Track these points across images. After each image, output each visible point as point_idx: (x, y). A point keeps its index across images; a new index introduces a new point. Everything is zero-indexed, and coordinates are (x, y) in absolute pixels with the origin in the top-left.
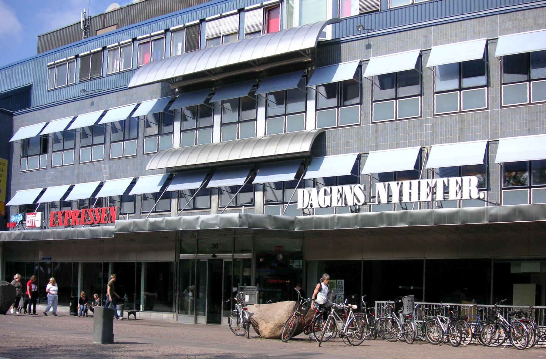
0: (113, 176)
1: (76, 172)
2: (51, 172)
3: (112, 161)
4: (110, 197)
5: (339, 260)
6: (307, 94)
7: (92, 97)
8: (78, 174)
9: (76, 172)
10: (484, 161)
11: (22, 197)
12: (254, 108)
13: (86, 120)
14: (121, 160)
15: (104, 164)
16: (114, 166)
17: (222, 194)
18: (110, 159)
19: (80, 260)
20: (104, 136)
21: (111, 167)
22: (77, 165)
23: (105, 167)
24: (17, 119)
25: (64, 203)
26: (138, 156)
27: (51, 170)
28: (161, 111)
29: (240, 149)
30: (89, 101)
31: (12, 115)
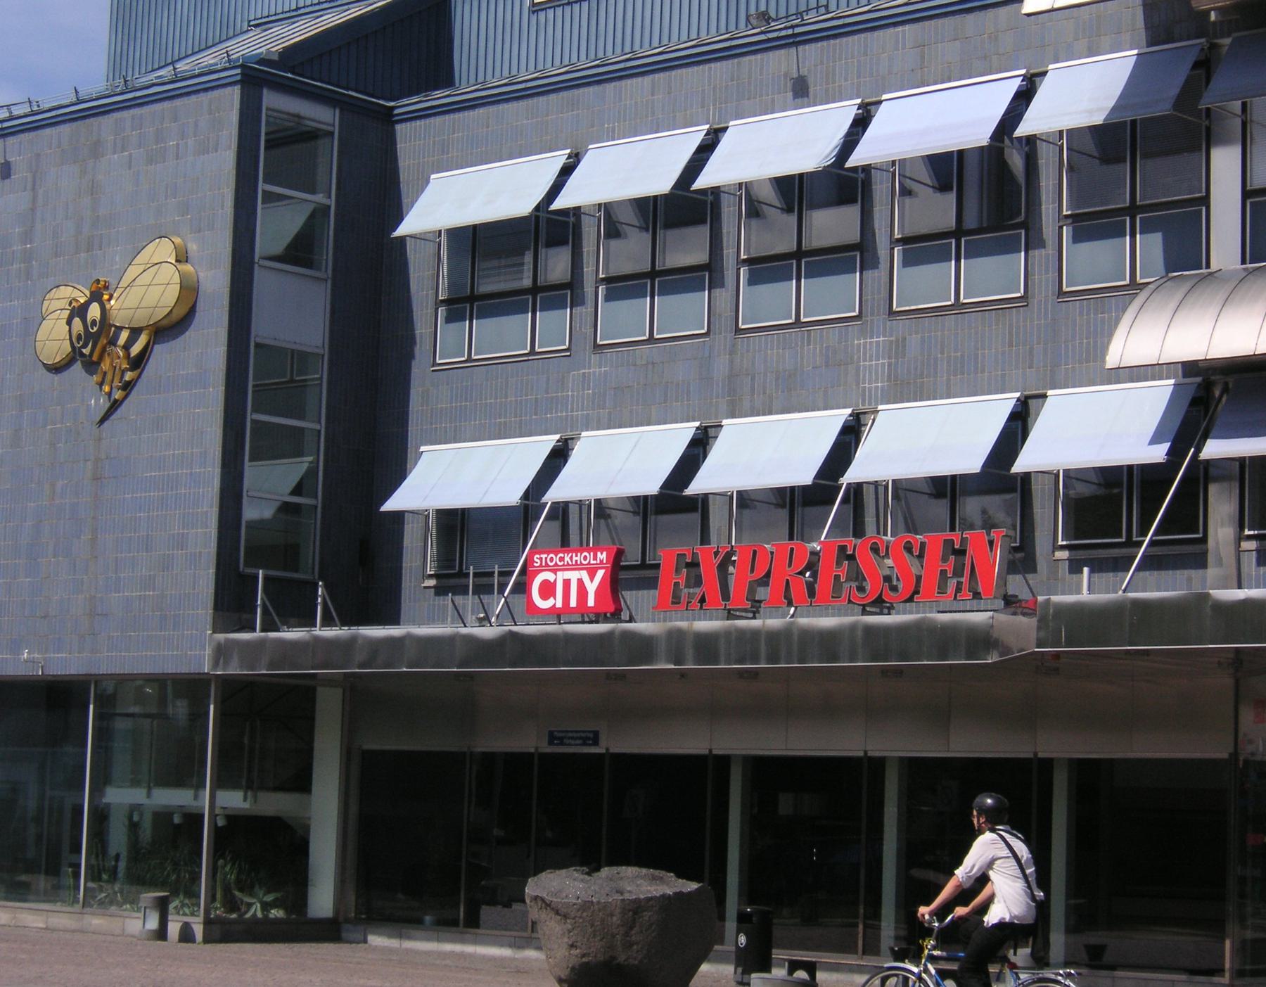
0: (910, 387)
1: (721, 366)
2: (596, 367)
3: (900, 325)
4: (598, 502)
5: (1197, 755)
6: (1208, 129)
7: (794, 41)
8: (732, 376)
9: (721, 366)
10: (821, 474)
11: (453, 474)
12: (1194, 148)
13: (774, 144)
14: (950, 321)
15: (863, 333)
16: (914, 341)
17: (609, 516)
18: (891, 313)
19: (895, 743)
20: (705, 230)
21: (897, 349)
22: (723, 338)
23: (870, 347)
24: (411, 140)
25: (674, 500)
26: (1034, 302)
27: (595, 358)
28: (1164, 108)
29: (1213, 311)
30: (780, 62)
31: (388, 119)
